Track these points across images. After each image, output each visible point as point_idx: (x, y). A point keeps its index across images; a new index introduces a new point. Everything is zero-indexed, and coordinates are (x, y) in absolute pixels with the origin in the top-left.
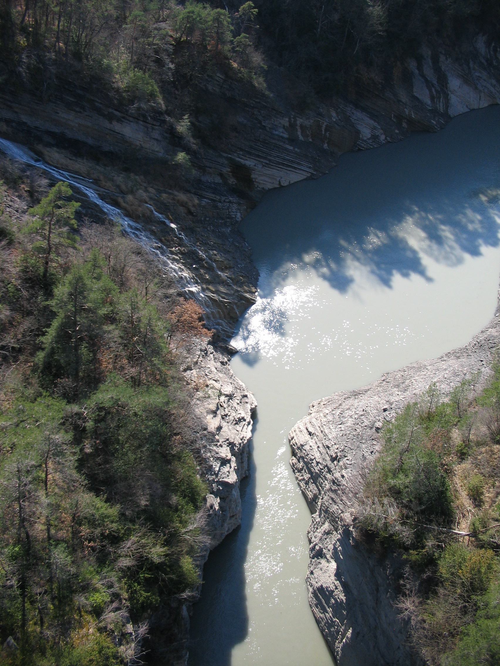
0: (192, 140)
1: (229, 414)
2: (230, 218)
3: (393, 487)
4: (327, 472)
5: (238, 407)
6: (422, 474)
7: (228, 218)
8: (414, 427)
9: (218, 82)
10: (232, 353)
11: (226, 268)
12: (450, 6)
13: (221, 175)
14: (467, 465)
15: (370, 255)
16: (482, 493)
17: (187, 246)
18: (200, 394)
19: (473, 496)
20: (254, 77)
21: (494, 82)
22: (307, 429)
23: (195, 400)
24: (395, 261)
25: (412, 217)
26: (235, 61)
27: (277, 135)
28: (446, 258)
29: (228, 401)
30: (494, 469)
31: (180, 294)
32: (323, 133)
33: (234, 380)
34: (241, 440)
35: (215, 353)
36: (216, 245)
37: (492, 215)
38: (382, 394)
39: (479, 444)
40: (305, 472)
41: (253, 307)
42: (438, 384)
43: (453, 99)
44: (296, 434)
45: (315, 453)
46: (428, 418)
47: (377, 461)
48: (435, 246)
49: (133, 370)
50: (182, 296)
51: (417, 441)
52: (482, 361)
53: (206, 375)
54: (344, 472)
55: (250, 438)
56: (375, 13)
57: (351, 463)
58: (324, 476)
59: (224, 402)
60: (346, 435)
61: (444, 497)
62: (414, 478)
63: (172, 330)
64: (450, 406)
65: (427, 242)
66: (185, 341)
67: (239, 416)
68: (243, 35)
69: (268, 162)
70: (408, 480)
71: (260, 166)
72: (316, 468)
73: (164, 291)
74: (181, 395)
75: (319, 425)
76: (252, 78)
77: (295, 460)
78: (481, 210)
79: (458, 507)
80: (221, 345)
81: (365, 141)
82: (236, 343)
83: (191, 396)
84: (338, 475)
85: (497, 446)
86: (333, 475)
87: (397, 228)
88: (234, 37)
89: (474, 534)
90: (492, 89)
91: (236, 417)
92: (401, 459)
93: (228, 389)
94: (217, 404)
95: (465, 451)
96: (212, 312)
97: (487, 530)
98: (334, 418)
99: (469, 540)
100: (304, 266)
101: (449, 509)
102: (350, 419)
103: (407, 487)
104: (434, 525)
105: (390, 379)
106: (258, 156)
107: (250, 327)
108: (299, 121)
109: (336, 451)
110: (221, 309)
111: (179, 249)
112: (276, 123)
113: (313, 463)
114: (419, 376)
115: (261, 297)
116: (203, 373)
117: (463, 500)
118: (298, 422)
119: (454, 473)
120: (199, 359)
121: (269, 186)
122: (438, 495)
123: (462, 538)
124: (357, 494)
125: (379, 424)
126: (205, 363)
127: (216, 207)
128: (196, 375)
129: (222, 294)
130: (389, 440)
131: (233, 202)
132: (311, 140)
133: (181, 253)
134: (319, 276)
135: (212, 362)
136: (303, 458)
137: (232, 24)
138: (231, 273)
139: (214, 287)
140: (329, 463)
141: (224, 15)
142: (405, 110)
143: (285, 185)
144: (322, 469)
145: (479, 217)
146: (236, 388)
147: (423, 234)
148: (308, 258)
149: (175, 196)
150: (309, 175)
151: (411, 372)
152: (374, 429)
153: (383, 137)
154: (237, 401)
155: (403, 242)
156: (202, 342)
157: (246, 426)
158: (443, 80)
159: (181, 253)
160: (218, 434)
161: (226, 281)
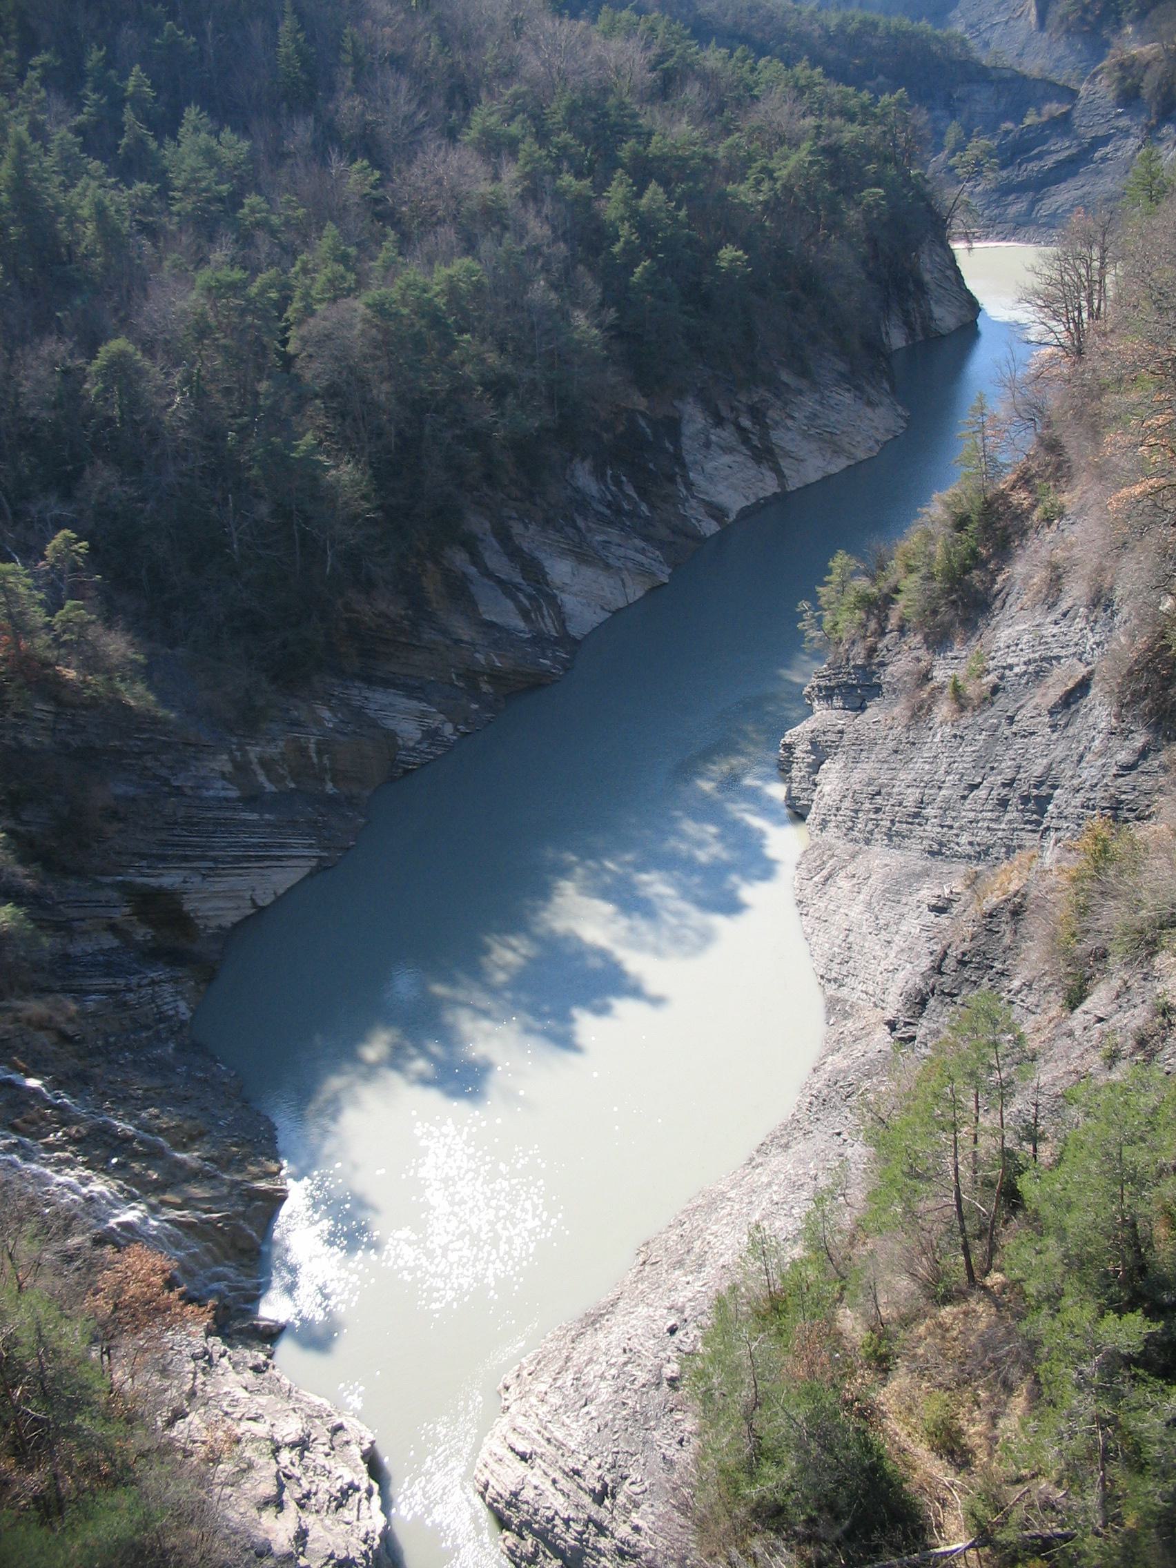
0: (19, 870)
1: (313, 1490)
2: (162, 1018)
3: (759, 1504)
4: (596, 1535)
5: (329, 1463)
6: (813, 1444)
7: (160, 1021)
8: (751, 1344)
9: (43, 721)
10: (271, 1335)
11: (193, 1139)
12: (496, 423)
13: (113, 928)
14: (900, 1380)
15: (508, 995)
16: (960, 1432)
17: (83, 1120)
18: (226, 1468)
19: (944, 1446)
20: (122, 687)
21: (638, 543)
22: (513, 1450)
23: (218, 1490)
24: (571, 987)
25: (568, 879)
26: (68, 667)
27: (213, 798)
28: (678, 941)
29: (302, 1457)
30: (963, 1364)
31: (99, 1241)
32: (315, 760)
33: (297, 1399)
34: (365, 1542)
35: (230, 1352)
36: (151, 1094)
37: (738, 815)
38: (652, 1296)
39: (907, 1322)
40: (546, 1556)
41: (285, 1210)
42: (765, 1224)
43: (569, 602)
44: (492, 1472)
45: (551, 1499)
46: (774, 1308)
47: (701, 1455)
48: (642, 925)
49: (35, 1477)
50: (106, 1243)
51: (771, 1372)
52: (839, 1134)
53: (226, 1414)
54: (635, 1518)
55: (385, 1527)
56: (346, 478)
57: (643, 1488)
58: (595, 1548)
59: (292, 1464)
60: (606, 1426)
61: (881, 1477)
62: (798, 1462)
63: (105, 1335)
64: (809, 1261)
65: (624, 922)
66: (147, 1350)
67: (339, 1484)
68: (70, 603)
69: (211, 865)
70: (785, 1475)
71: (198, 879)
72: (568, 1537)
73: (56, 1246)
74: (181, 1491)
75: (537, 1427)
76: (118, 690)
77: (512, 1539)
78: (709, 811)
79: (921, 1487)
80: (239, 1325)
81: (414, 749)
82: (274, 1308)
83: (203, 1481)
84: (623, 1531)
85: (948, 1308)
86: (613, 1536)
87: (545, 915)
88: (51, 614)
89: (983, 1537)
90: (640, 558)
91: (333, 1491)
92: (751, 1428)
93: (290, 1429)
94: (278, 1478)
95: (883, 1350)
96: (193, 1255)
97: (1007, 1515)
98: (565, 1397)
99: (978, 1555)
100: (370, 1072)
101: (904, 1502)
102: (603, 1385)
103: (791, 1489)
104: (888, 1555)
105: (657, 1253)
106: (186, 858)
107: (292, 1258)
108: (254, 752)
109: (599, 1473)
110: (211, 1241)
111: (65, 1134)
112: (202, 773)
113: (554, 1526)
114: (717, 1221)
115: (298, 1178)
116: (216, 1411)
117: (928, 1467)
118: (486, 1440)
119: (881, 1411)
120: (198, 1382)
121: (231, 918)
122: (867, 1477)
123: (962, 1561)
124: (685, 1558)
125: (671, 1369)
126: (213, 1385)
127: (124, 1005)
128: (203, 1425)
129: (201, 1204)
130: (708, 1396)
131: (161, 981)
132: (293, 785)
133: (74, 1141)
134: (412, 1083)
135: (232, 1375)
136: (527, 1524)
137: (38, 588)
138: (208, 1146)
139: (177, 1194)
140: (593, 1509)
141: (15, 573)
142: (477, 655)
143: (268, 902)
144: (584, 1533)
145: (712, 829)
146: (309, 1416)
147: (608, 908)
148: (372, 1052)
149: (20, 1010)
150: (313, 863)
151: (698, 1220)
152: (665, 1384)
153: (448, 729)
154: (321, 1448)
155: (571, 938)
156: (191, 1335)
157: (364, 1502)
158: (533, 571)
159: (74, 1141)
160: (302, 1554)
161: (201, 1170)
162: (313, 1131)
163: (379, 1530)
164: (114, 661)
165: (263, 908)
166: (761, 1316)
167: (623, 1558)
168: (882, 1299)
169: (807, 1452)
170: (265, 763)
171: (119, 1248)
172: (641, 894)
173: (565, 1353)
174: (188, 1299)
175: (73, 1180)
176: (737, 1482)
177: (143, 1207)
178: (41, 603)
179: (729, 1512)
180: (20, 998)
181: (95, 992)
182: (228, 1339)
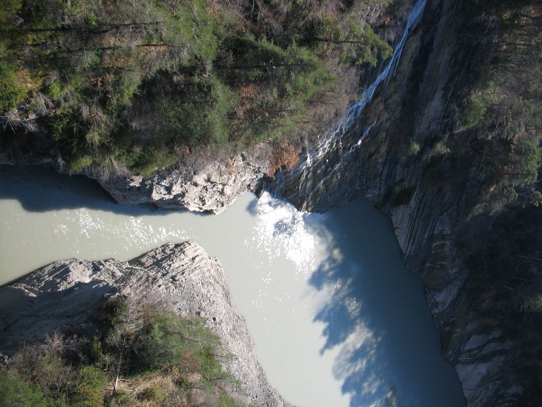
0: (430, 156)
3: (152, 327)
5: (214, 199)
7: (367, 187)
8: (201, 343)
9: (478, 175)
10: (258, 193)
11: (326, 187)
13: (402, 180)
14: (172, 387)
16: (149, 400)
17: (343, 154)
18: (223, 168)
19: (147, 393)
20: (483, 205)
21: (485, 401)
23: (218, 164)
24: (336, 324)
26: (495, 189)
28: (340, 366)
31: (304, 150)
35: (257, 179)
36: (345, 178)
37: (375, 402)
39: (189, 396)
42: (237, 361)
43: (470, 368)
45: (178, 263)
46: (209, 354)
47: (173, 314)
48: (349, 356)
49: (242, 113)
51: (190, 346)
52: (257, 397)
58: (159, 271)
61: (145, 369)
63: (275, 144)
65: (352, 350)
67: (206, 200)
68: (517, 195)
69: (414, 218)
70: (158, 339)
72: (166, 264)
73: (307, 136)
75: (201, 266)
76: (482, 204)
77: (171, 247)
78: (380, 393)
79: (137, 380)
80: (264, 184)
81: (433, 297)
82: (265, 196)
83: (222, 161)
84: (161, 282)
88: (515, 188)
90: (479, 400)
91: (205, 198)
93: (228, 191)
94: (215, 182)
96: (290, 176)
100: (330, 250)
102: (206, 291)
106: (418, 210)
108: (448, 243)
109: (180, 280)
111: (340, 148)
114: (243, 346)
117: (143, 385)
121: (394, 219)
125: (203, 314)
127: (376, 177)
130: (190, 323)
132: (433, 252)
135: (250, 178)
136: (174, 253)
137: (525, 186)
139: (311, 177)
140: (170, 275)
141: (533, 179)
143: (396, 233)
145: (373, 391)
147: (358, 346)
149: (384, 144)
150: (404, 252)
151: (246, 340)
154: (219, 198)
155: (352, 330)
156: (266, 169)
157: (198, 206)
158: (484, 359)
159: (337, 150)
161: (316, 186)
162: (316, 225)
163: (189, 208)
164: (492, 205)
165: (394, 231)
166: (209, 349)
167: (153, 279)
168: (198, 390)
169: (162, 348)
170: (443, 245)
171: (300, 155)
172: (359, 359)
173: (220, 282)
174: (278, 171)
175: (325, 147)
176: (161, 322)
177: (310, 165)
178: (520, 185)
179: (154, 317)
180: (388, 145)
181: (383, 169)
182: (261, 180)
